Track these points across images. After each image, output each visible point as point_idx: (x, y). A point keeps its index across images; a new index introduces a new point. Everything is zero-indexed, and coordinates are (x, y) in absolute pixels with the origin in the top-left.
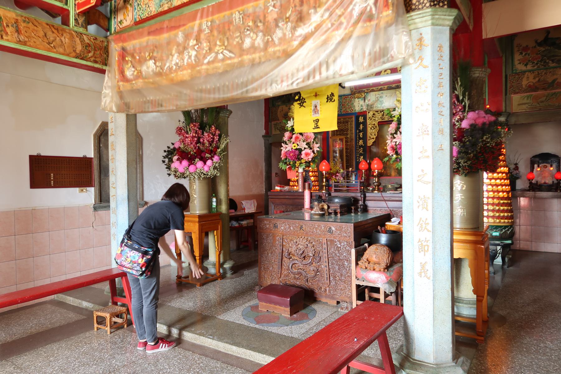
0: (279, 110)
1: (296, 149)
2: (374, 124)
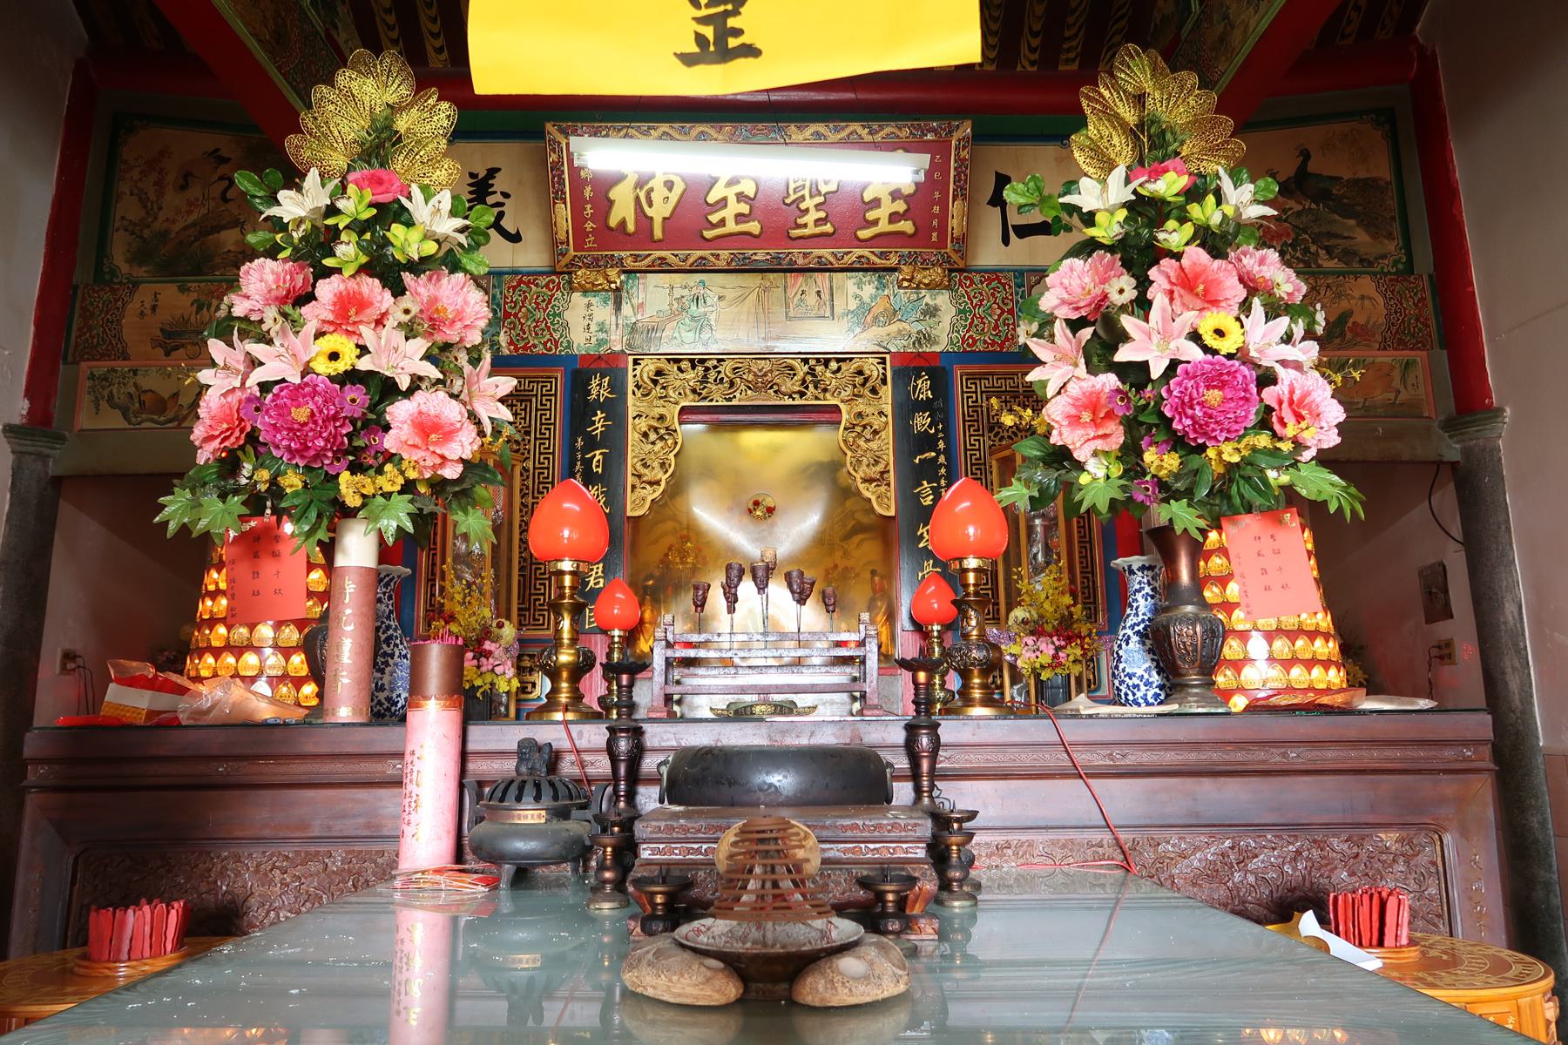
0: (133, 307)
1: (352, 377)
2: (662, 418)
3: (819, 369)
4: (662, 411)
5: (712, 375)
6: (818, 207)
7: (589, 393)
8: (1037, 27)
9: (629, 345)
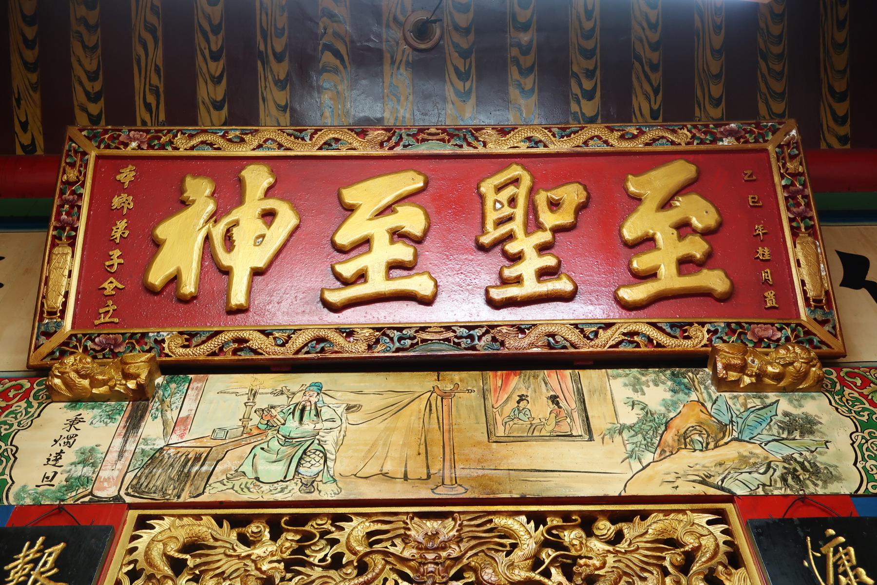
3: (571, 536)
5: (318, 553)
6: (543, 249)
8: (840, 86)
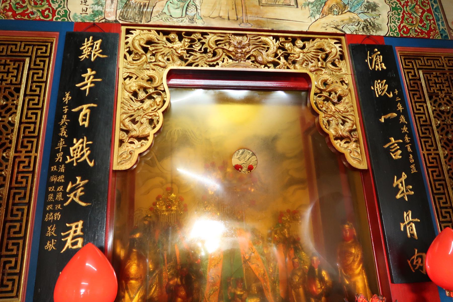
2: (151, 79)
3: (288, 45)
4: (151, 73)
5: (197, 46)
7: (81, 53)
9: (123, 17)
